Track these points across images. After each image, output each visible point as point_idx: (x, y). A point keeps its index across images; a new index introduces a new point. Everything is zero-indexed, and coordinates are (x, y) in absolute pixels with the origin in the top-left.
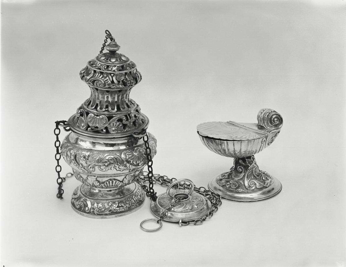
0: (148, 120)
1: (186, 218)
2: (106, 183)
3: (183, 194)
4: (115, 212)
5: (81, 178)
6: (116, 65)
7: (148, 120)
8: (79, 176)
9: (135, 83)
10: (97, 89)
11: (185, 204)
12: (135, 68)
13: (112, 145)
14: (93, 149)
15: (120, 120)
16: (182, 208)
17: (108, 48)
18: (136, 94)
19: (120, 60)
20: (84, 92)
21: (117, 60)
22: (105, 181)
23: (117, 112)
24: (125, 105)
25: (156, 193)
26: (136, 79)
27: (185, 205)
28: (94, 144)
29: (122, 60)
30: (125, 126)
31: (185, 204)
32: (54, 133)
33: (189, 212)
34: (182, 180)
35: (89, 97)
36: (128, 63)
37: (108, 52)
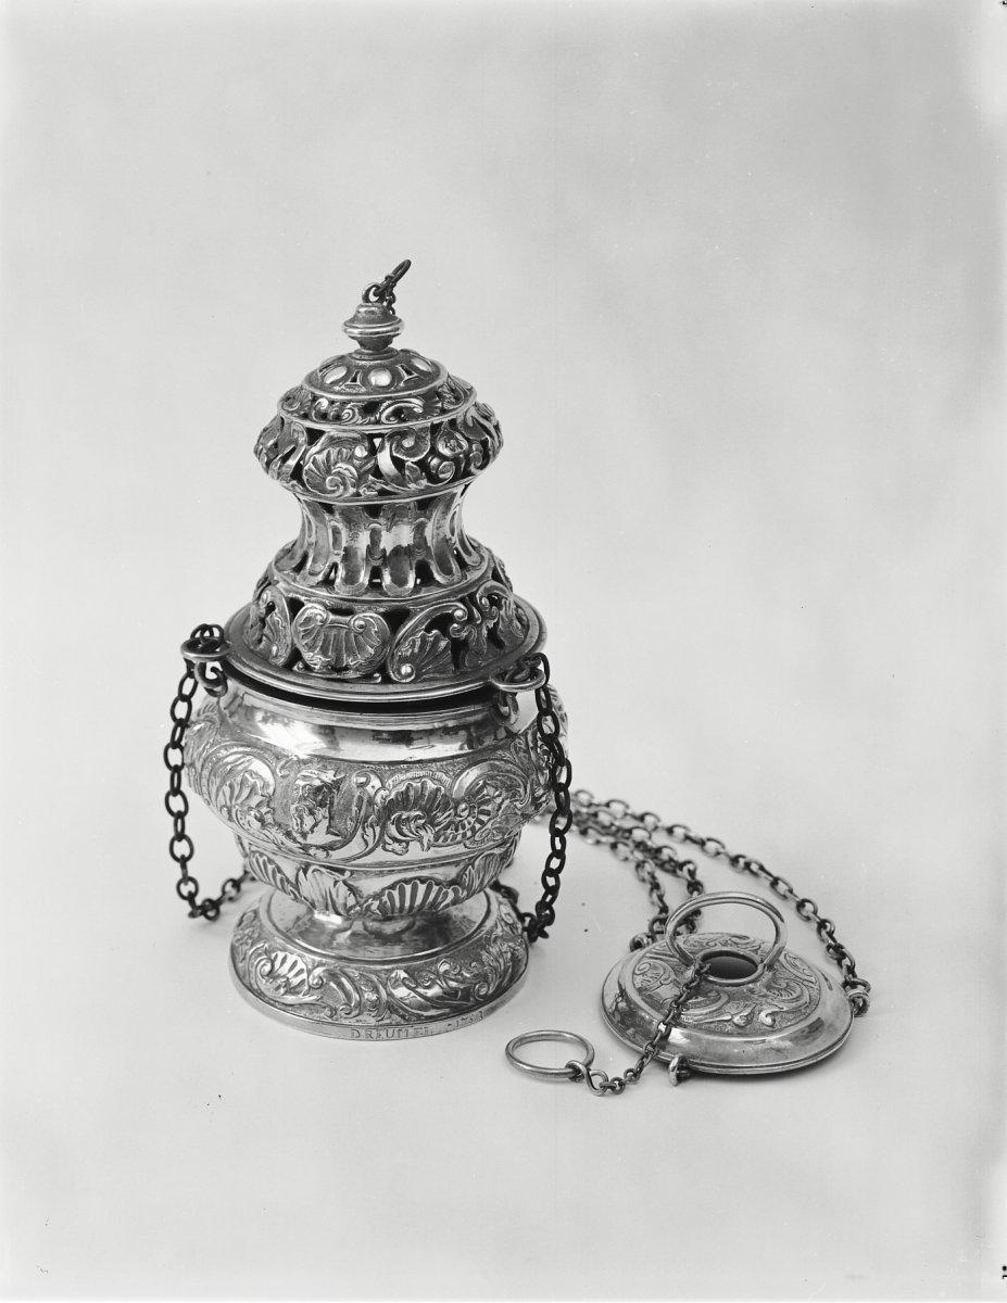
0: (538, 618)
1: (707, 1057)
2: (391, 897)
3: (743, 957)
4: (396, 1012)
5: (279, 876)
6: (321, 433)
7: (538, 618)
8: (270, 867)
9: (479, 465)
10: (329, 509)
11: (724, 998)
12: (471, 401)
13: (404, 738)
14: (332, 754)
15: (442, 622)
16: (705, 1012)
17: (356, 331)
18: (484, 512)
19: (409, 373)
20: (280, 516)
21: (396, 377)
22: (383, 890)
23: (417, 588)
24: (451, 559)
25: (545, 935)
26: (479, 443)
27: (719, 1004)
28: (328, 732)
29: (417, 370)
30: (458, 647)
31: (724, 998)
32: (178, 684)
33: (729, 1034)
34: (736, 895)
35: (294, 534)
36: (437, 383)
37: (356, 346)
